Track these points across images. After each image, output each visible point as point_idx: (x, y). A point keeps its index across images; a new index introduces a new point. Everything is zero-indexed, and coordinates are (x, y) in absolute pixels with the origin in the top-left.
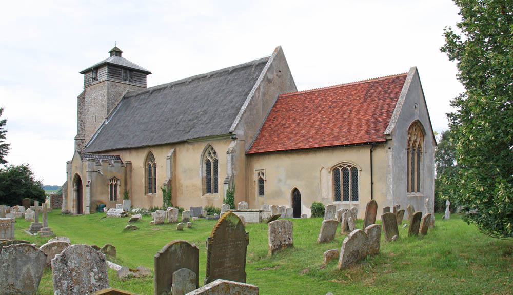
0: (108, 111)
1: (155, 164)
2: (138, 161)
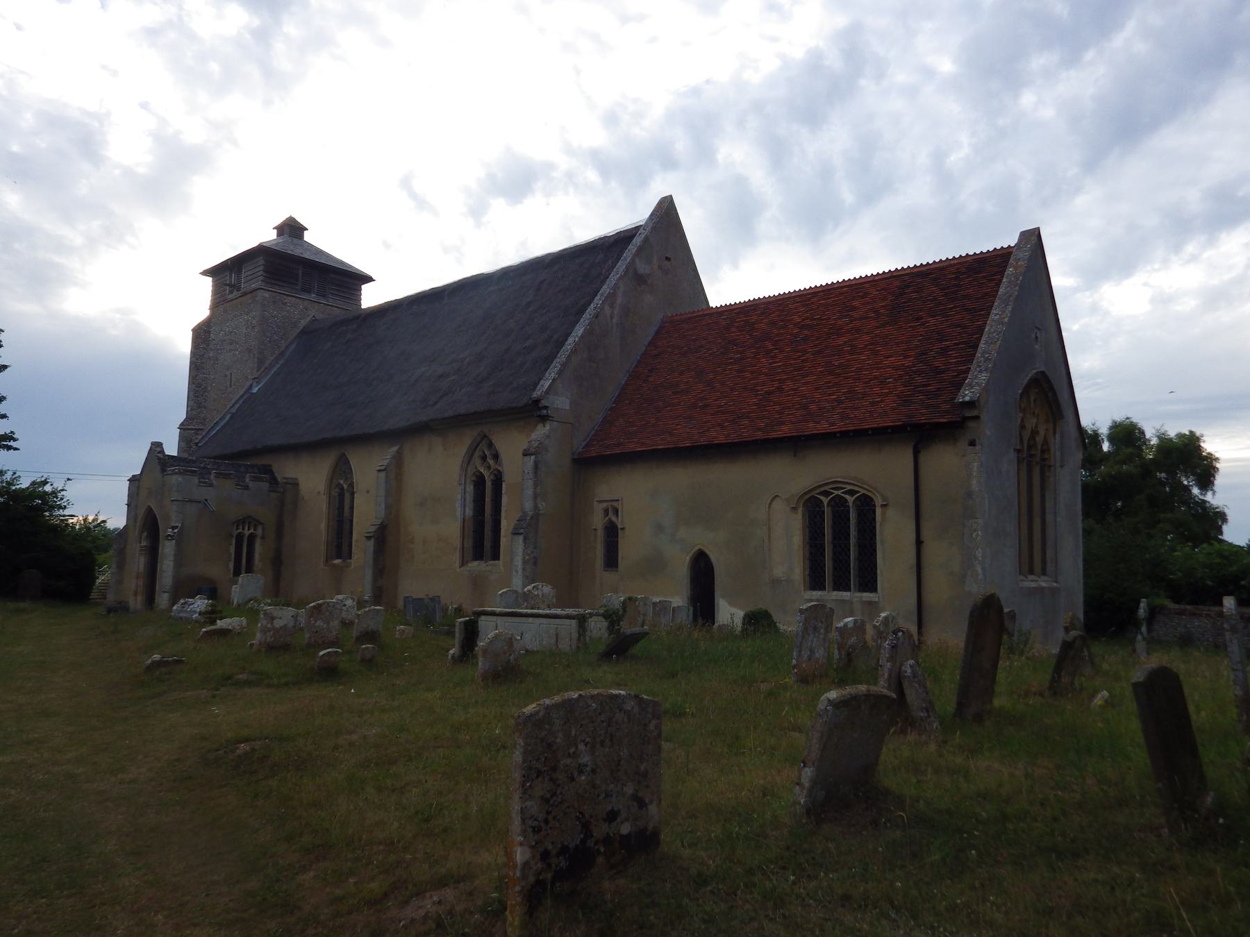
0: (261, 361)
1: (351, 485)
2: (311, 477)
